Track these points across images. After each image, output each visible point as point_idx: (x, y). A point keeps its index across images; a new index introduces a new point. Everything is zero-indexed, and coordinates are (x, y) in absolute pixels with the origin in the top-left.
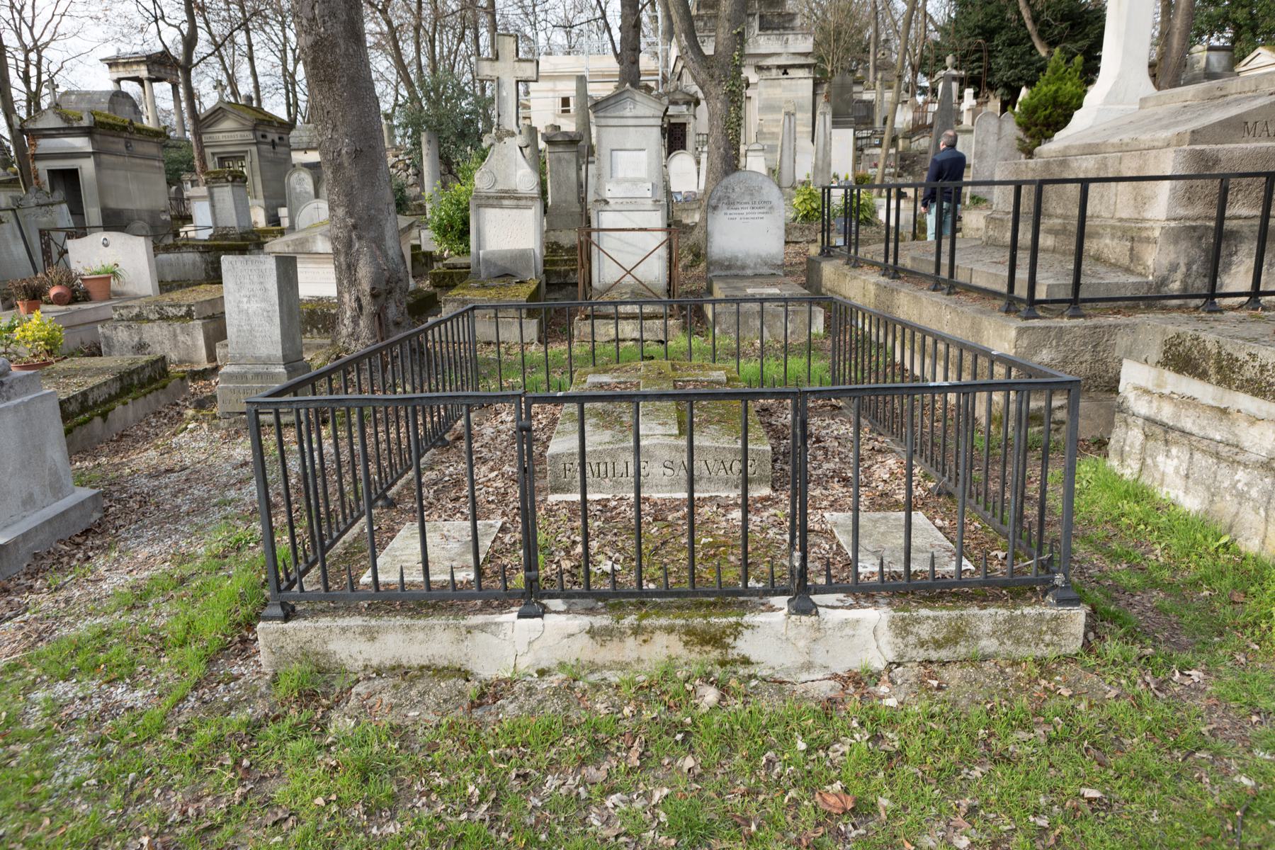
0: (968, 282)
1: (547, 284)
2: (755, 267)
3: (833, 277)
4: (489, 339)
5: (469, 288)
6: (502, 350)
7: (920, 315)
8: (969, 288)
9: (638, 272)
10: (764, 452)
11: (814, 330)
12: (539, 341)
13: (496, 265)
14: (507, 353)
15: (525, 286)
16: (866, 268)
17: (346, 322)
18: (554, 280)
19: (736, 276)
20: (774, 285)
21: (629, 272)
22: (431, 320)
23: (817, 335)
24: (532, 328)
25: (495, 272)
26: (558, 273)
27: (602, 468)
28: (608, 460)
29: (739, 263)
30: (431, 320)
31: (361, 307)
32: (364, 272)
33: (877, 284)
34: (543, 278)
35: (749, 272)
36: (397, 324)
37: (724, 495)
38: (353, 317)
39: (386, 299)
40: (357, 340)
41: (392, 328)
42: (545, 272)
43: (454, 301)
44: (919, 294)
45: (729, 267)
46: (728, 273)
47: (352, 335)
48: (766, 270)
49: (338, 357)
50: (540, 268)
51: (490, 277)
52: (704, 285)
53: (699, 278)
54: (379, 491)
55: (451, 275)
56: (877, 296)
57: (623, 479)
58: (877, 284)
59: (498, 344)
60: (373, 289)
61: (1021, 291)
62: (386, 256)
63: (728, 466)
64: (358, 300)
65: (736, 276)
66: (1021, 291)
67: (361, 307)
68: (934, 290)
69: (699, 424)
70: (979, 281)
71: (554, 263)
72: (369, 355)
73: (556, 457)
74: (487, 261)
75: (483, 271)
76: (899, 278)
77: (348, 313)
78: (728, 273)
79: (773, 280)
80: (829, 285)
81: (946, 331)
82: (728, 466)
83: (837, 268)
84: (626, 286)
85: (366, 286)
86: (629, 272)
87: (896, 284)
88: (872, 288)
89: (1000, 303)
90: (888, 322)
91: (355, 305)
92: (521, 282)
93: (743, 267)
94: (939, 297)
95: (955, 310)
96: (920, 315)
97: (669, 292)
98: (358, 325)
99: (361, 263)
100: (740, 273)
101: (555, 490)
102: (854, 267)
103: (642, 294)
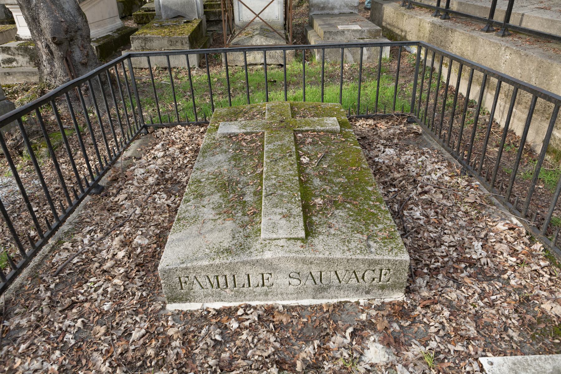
0: (517, 25)
1: (208, 21)
2: (340, 9)
3: (392, 15)
4: (164, 66)
5: (150, 28)
6: (173, 74)
7: (475, 52)
8: (519, 31)
9: (264, 16)
10: (401, 262)
11: (383, 56)
12: (200, 66)
13: (171, 9)
14: (176, 78)
15: (190, 24)
16: (417, 9)
17: (45, 63)
18: (212, 18)
19: (328, 15)
20: (354, 22)
21: (257, 16)
22: (124, 53)
23: (385, 59)
24: (194, 59)
25: (171, 14)
26: (214, 13)
27: (222, 280)
28: (227, 273)
29: (330, 6)
30: (124, 53)
31: (51, 53)
32: (45, 23)
33: (433, 24)
34: (204, 18)
35: (336, 11)
36: (85, 65)
37: (353, 300)
38: (48, 60)
39: (70, 45)
40: (55, 77)
41: (80, 67)
42: (205, 13)
43: (138, 38)
44: (475, 34)
45: (323, 8)
46: (323, 12)
47: (51, 73)
48: (347, 10)
49: (43, 92)
50: (201, 10)
51: (167, 19)
52: (307, 19)
53: (303, 14)
54: (137, 131)
55: (147, 16)
56: (431, 32)
57: (245, 289)
58: (433, 24)
59: (170, 69)
60: (54, 38)
61: (499, 17)
62: (62, 9)
63: (360, 275)
64: (47, 46)
65: (328, 15)
66: (499, 17)
67: (51, 53)
68: (488, 31)
69: (323, 209)
70: (527, 24)
71: (212, 6)
72: (65, 90)
73: (168, 272)
74: (165, 7)
75: (163, 14)
76: (449, 19)
77: (44, 57)
78: (323, 12)
79: (353, 17)
80: (389, 21)
81: (503, 69)
82: (360, 275)
83: (396, 9)
84: (257, 23)
85: (49, 37)
86: (257, 16)
87: (448, 24)
88: (428, 27)
89: (483, 26)
90: (440, 55)
91: (46, 51)
92: (188, 22)
93: (332, 8)
94: (493, 37)
95: (517, 52)
96: (475, 52)
97: (285, 26)
98: (54, 66)
99: (42, 16)
100: (331, 12)
101: (173, 299)
102: (409, 8)
103: (267, 29)
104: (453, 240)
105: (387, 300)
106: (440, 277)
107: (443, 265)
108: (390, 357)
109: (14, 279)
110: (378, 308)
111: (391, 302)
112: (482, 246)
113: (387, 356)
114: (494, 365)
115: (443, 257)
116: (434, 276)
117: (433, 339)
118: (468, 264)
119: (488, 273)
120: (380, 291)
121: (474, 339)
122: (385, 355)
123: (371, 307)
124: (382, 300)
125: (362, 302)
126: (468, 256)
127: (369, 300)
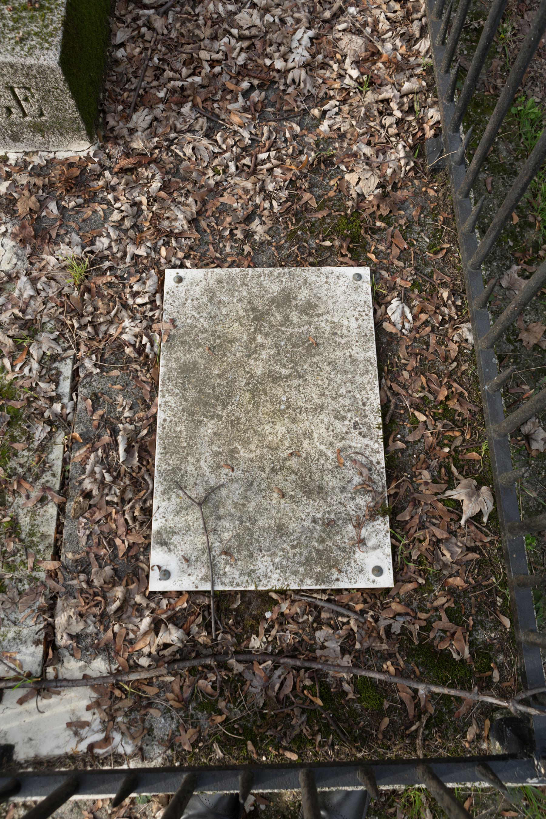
104: (258, 22)
105: (61, 155)
106: (186, 109)
107: (206, 83)
108: (19, 263)
109: (476, 70)
110: (38, 171)
111: (67, 159)
112: (311, 39)
113: (14, 261)
114: (184, 283)
115: (213, 63)
116: (174, 107)
117: (105, 234)
118: (256, 82)
119: (288, 104)
120: (39, 136)
121: (178, 236)
122: (11, 259)
123: (26, 167)
124: (52, 155)
125: (13, 157)
126: (268, 62)
127: (27, 154)
